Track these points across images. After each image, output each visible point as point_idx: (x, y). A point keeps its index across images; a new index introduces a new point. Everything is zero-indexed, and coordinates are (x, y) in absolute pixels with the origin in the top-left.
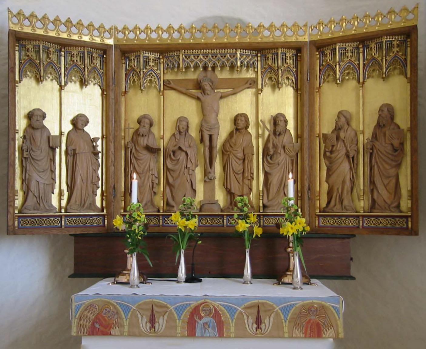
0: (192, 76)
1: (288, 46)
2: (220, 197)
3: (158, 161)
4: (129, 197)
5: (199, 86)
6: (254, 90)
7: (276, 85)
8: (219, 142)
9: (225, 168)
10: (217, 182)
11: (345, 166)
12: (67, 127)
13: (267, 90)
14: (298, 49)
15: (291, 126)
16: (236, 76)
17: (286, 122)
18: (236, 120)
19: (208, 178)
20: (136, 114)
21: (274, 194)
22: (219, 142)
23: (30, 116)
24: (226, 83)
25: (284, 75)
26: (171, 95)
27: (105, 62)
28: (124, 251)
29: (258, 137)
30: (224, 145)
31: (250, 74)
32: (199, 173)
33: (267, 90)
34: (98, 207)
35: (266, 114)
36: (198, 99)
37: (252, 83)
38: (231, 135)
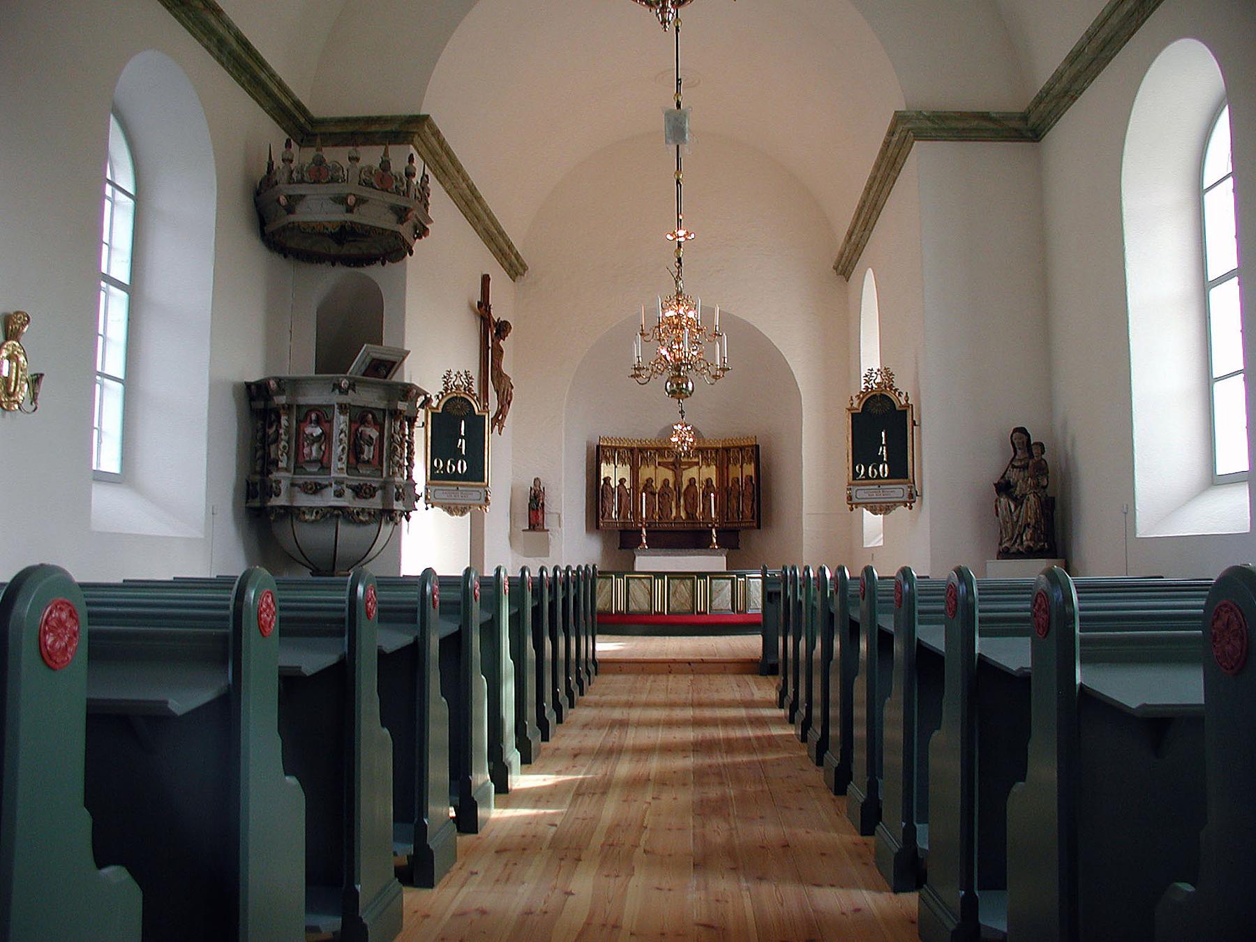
0: (671, 460)
1: (713, 449)
2: (683, 514)
3: (655, 498)
4: (462, 628)
5: (673, 464)
6: (698, 467)
7: (708, 465)
8: (683, 491)
9: (685, 501)
10: (681, 508)
11: (734, 502)
12: (618, 483)
13: (704, 467)
14: (717, 450)
15: (714, 483)
16: (690, 460)
17: (712, 481)
18: (690, 480)
19: (678, 507)
20: (646, 477)
21: (479, 311)
22: (683, 491)
23: (605, 479)
24: (686, 463)
25: (1106, 50)
26: (660, 468)
27: (632, 454)
28: (870, 267)
29: (700, 487)
30: (685, 491)
31: (696, 460)
32: (673, 504)
33: (704, 467)
34: (1234, 180)
35: (703, 478)
36: (673, 470)
37: (697, 464)
38: (688, 487)
